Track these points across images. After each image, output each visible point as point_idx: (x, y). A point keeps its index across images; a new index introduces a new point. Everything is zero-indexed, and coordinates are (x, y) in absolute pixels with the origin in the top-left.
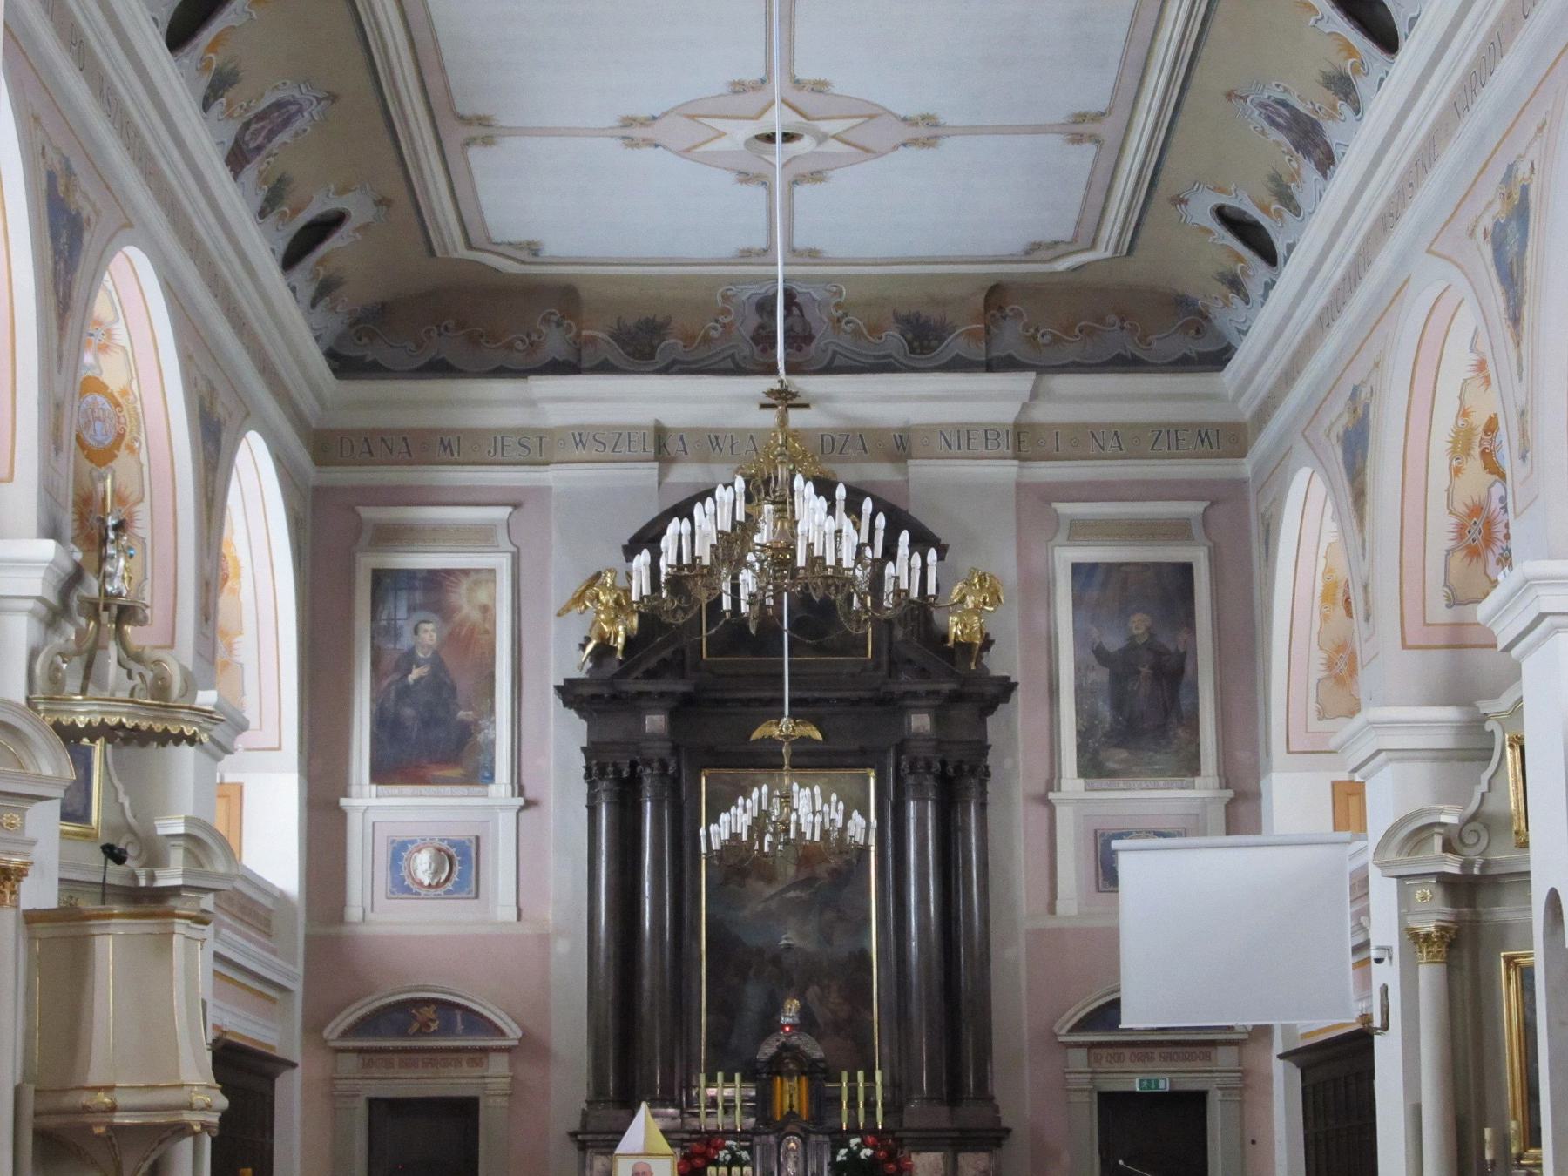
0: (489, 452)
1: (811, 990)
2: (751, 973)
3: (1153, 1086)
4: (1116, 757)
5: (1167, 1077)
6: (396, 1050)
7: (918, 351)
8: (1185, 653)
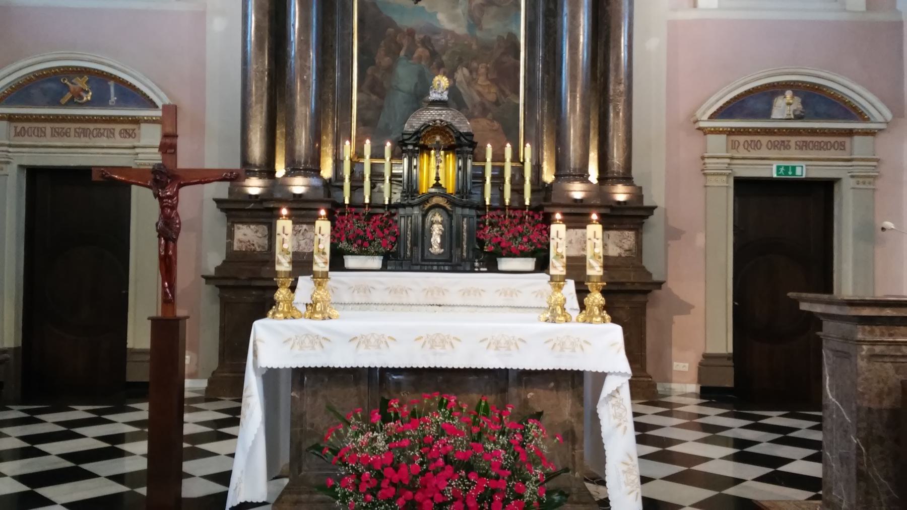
1: (459, 71)
2: (402, 53)
5: (803, 164)
6: (48, 119)
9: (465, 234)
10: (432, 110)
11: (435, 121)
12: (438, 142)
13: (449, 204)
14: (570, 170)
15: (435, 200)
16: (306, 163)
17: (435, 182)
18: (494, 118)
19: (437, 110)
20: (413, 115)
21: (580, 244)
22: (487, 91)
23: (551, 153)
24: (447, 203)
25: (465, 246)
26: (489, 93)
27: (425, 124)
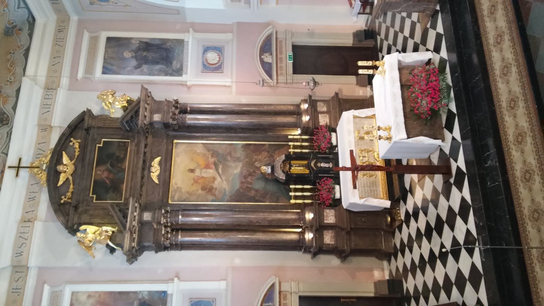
0: (18, 295)
2: (250, 186)
3: (291, 57)
4: (175, 64)
7: (7, 122)
8: (140, 41)
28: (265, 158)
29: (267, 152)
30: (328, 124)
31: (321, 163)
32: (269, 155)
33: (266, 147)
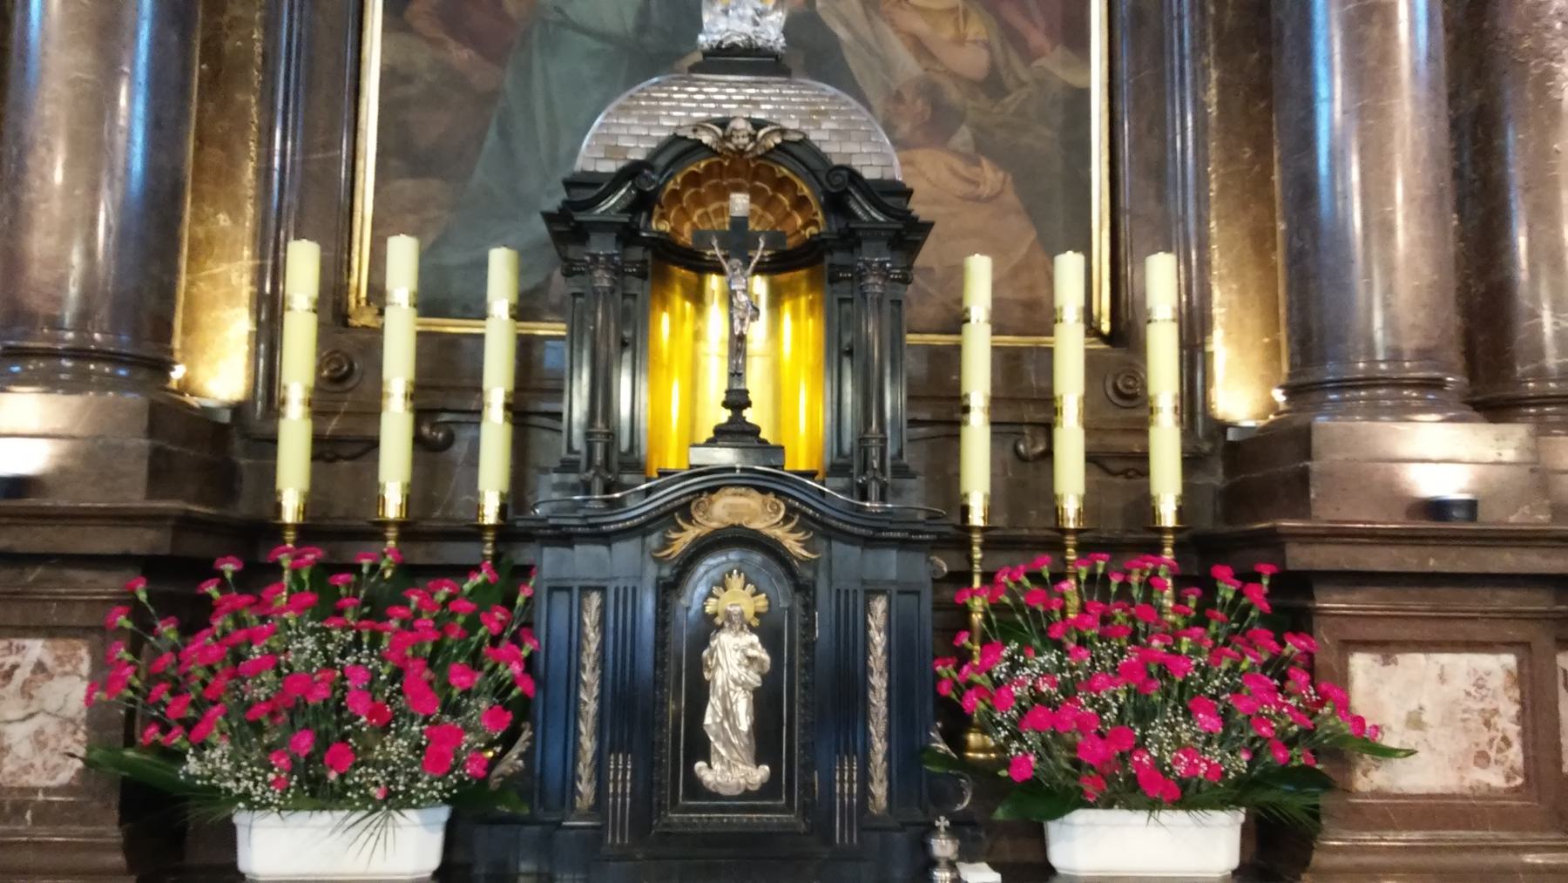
9: (878, 682)
10: (712, 83)
11: (723, 123)
12: (739, 224)
13: (792, 531)
14: (1372, 361)
15: (727, 508)
16: (84, 318)
17: (724, 415)
18: (983, 148)
19: (730, 84)
20: (622, 100)
21: (1467, 731)
22: (948, 32)
23: (1242, 291)
24: (787, 519)
25: (879, 747)
26: (960, 41)
27: (676, 139)
28: (919, 46)
29: (993, 68)
30: (1371, 779)
31: (768, 630)
32: (954, 95)
33: (1053, 62)
